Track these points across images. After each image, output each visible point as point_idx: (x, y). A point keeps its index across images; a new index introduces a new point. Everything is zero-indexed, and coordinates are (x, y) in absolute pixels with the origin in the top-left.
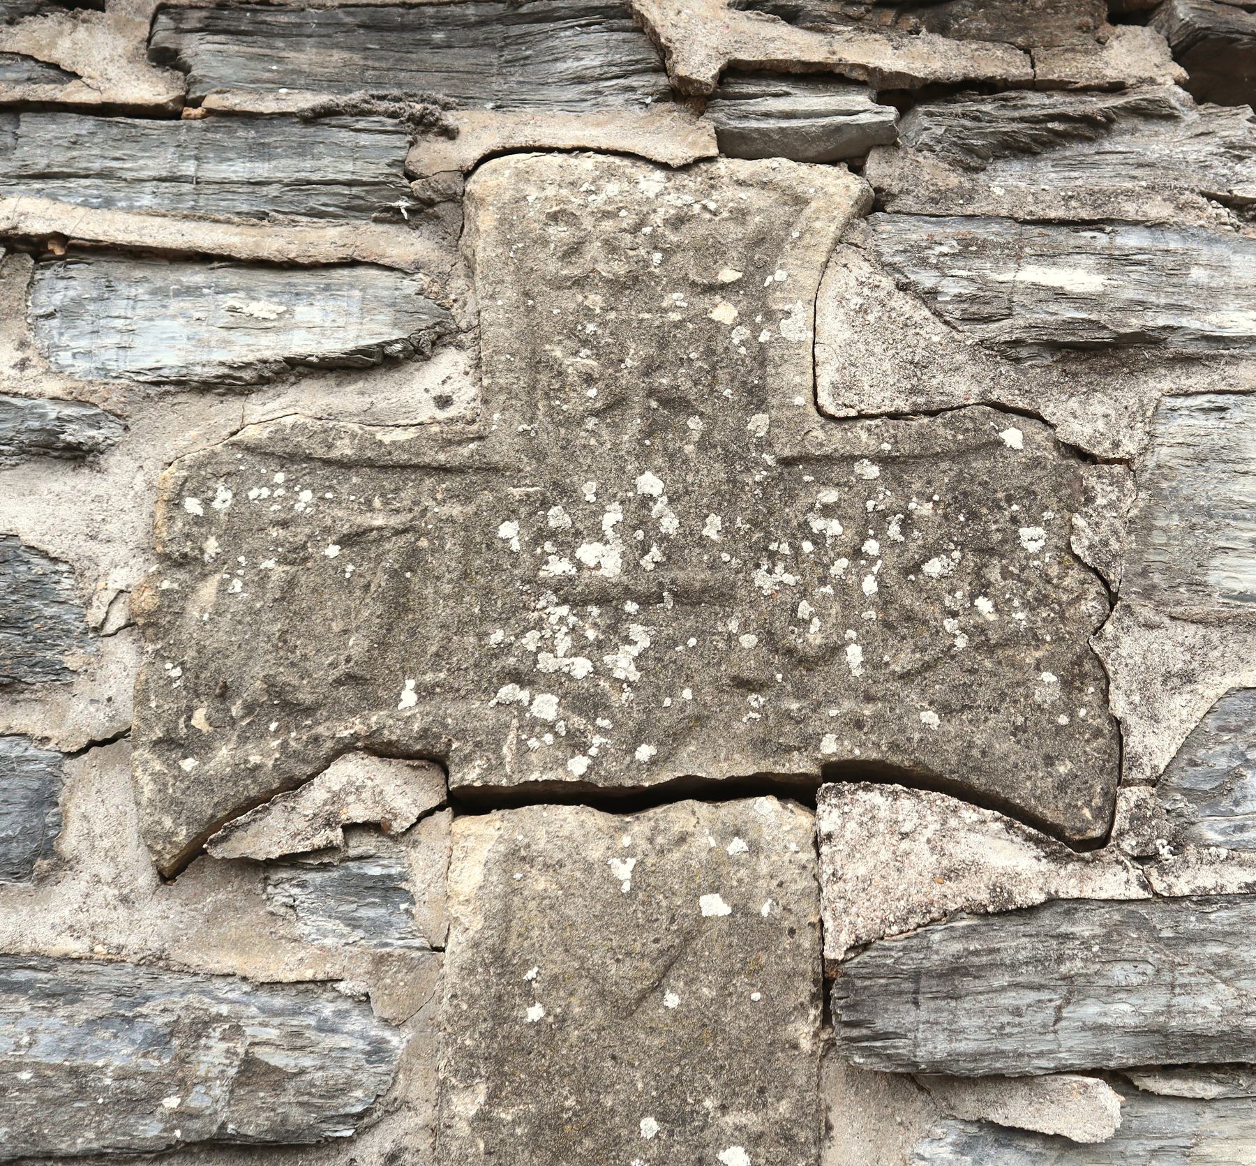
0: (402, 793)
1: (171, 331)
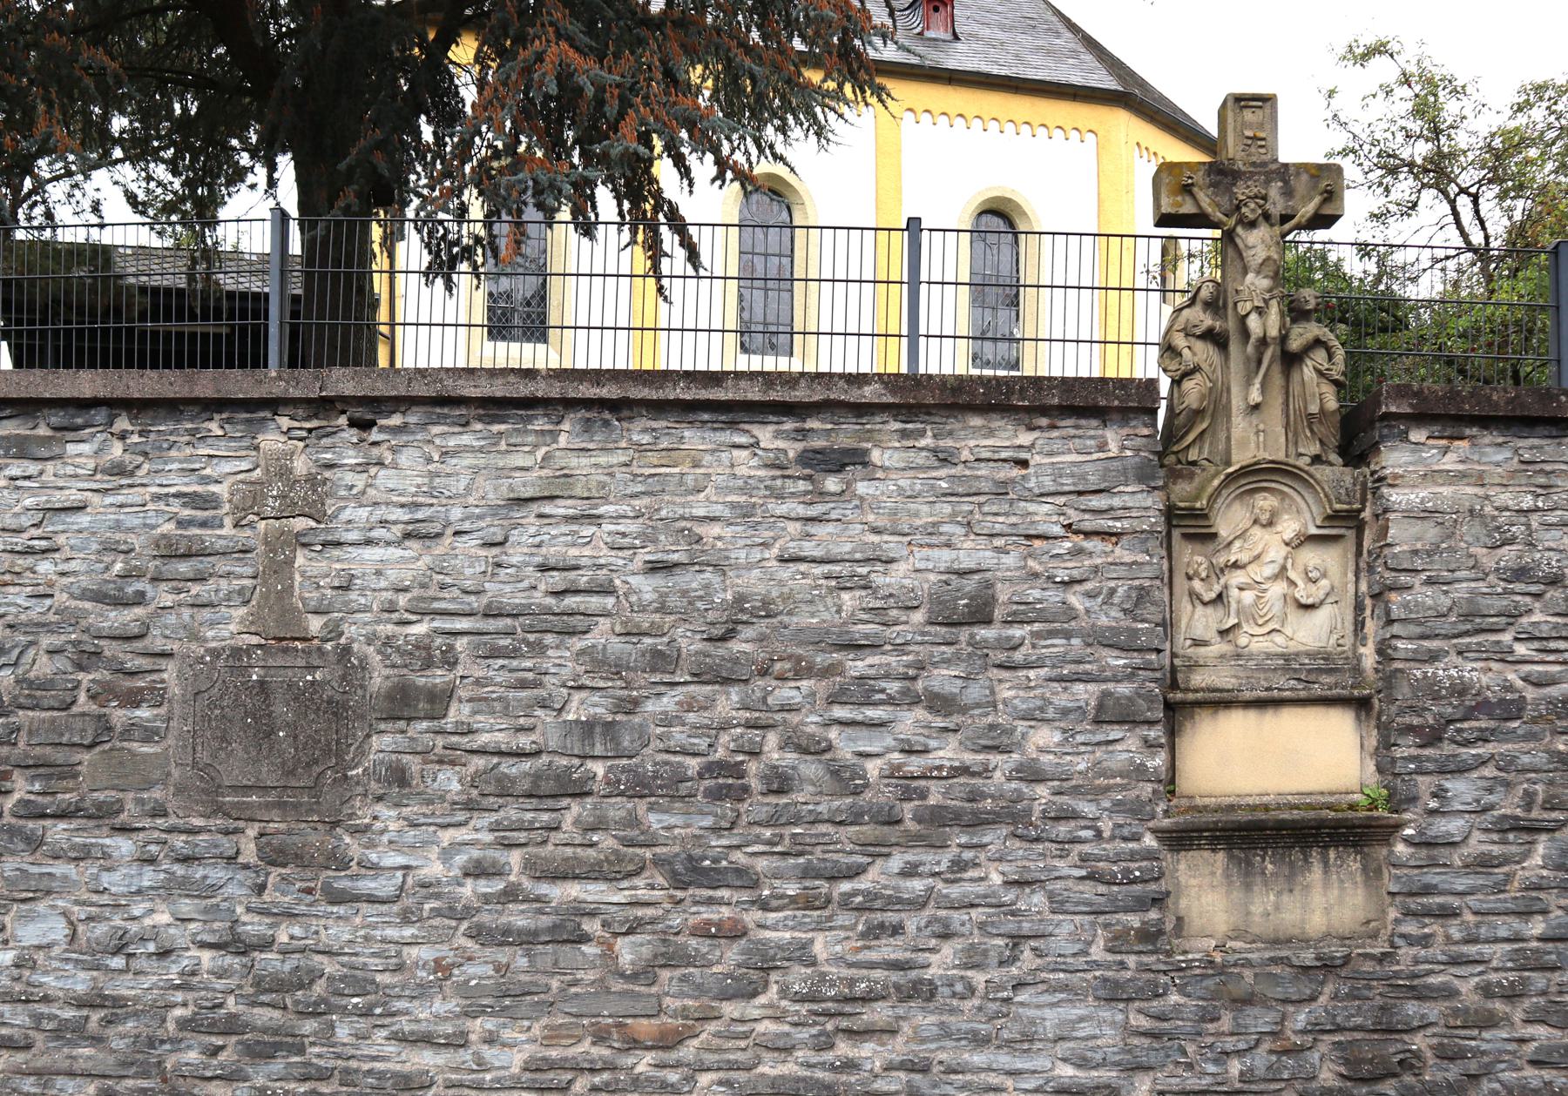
0: (256, 518)
1: (227, 467)
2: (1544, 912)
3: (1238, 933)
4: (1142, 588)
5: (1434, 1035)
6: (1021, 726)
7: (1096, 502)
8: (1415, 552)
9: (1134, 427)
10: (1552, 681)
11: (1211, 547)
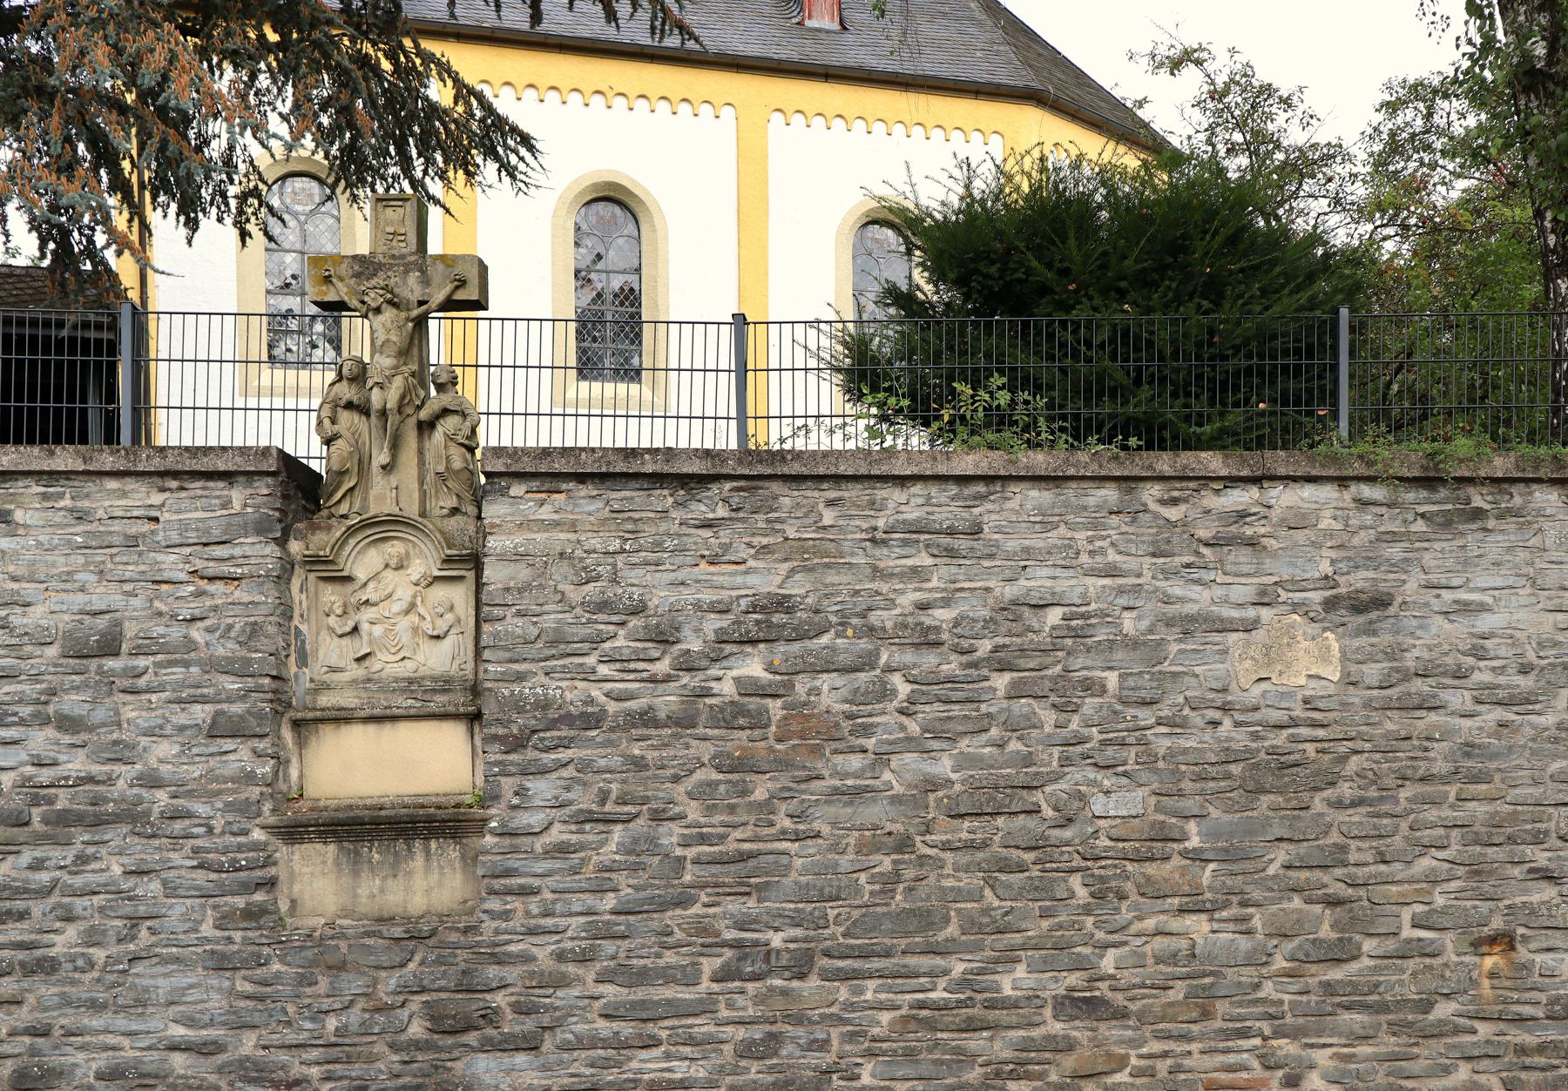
2: (615, 890)
3: (346, 913)
4: (255, 623)
6: (144, 741)
7: (219, 551)
8: (508, 589)
11: (350, 588)
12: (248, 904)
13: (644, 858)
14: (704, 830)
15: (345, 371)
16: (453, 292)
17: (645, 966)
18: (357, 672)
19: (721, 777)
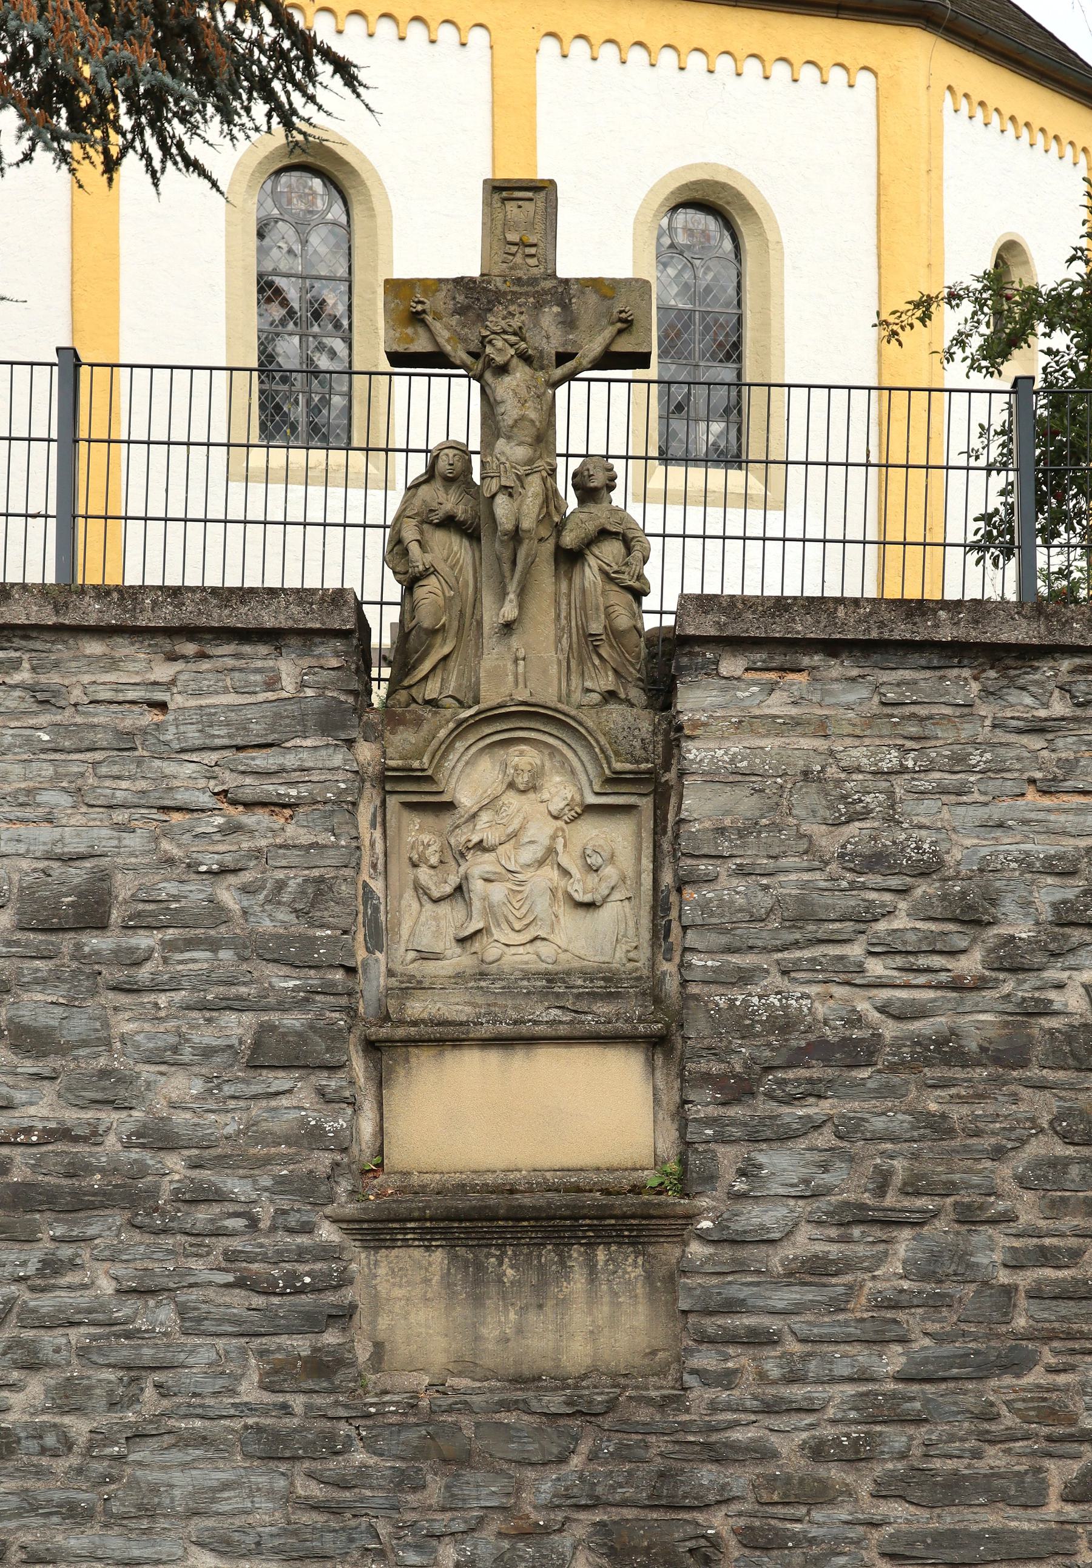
2: (903, 1341)
3: (464, 1366)
4: (321, 880)
5: (740, 1514)
6: (147, 1071)
7: (262, 760)
8: (721, 831)
9: (319, 656)
10: (920, 1012)
11: (448, 821)
12: (315, 1350)
13: (948, 1288)
14: (1047, 1241)
15: (443, 465)
16: (613, 341)
17: (955, 1472)
18: (457, 960)
19: (1070, 1151)
